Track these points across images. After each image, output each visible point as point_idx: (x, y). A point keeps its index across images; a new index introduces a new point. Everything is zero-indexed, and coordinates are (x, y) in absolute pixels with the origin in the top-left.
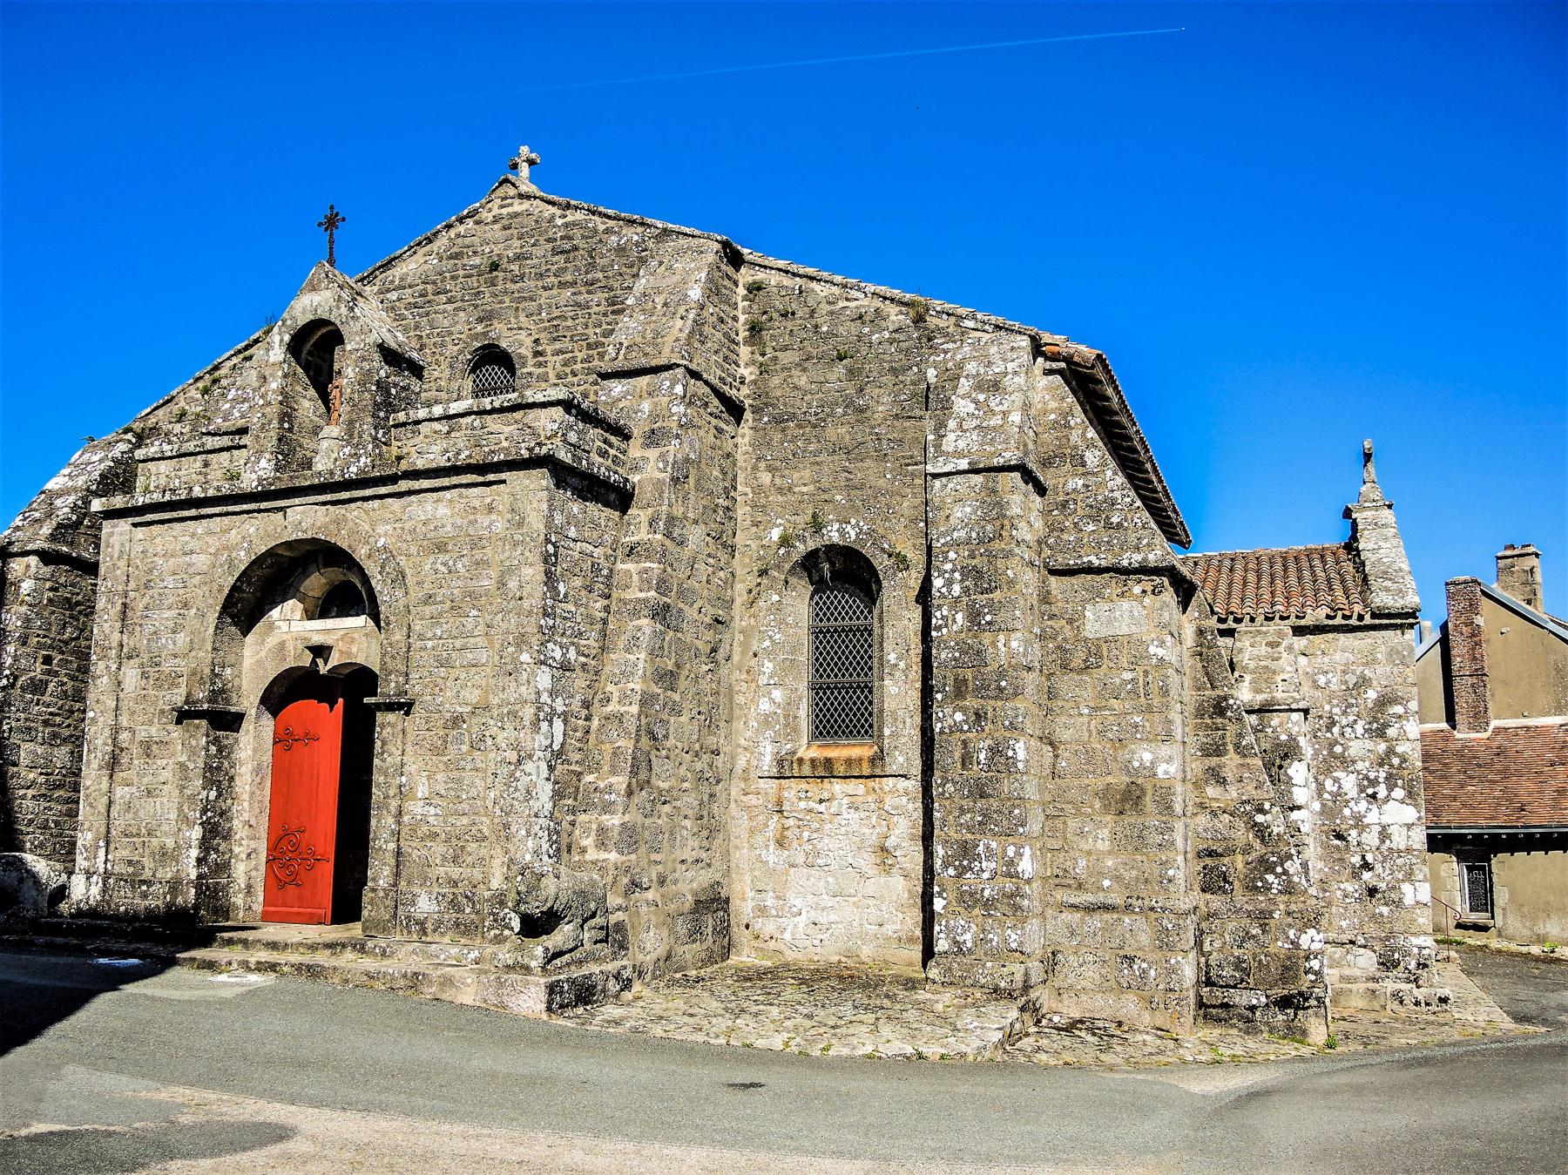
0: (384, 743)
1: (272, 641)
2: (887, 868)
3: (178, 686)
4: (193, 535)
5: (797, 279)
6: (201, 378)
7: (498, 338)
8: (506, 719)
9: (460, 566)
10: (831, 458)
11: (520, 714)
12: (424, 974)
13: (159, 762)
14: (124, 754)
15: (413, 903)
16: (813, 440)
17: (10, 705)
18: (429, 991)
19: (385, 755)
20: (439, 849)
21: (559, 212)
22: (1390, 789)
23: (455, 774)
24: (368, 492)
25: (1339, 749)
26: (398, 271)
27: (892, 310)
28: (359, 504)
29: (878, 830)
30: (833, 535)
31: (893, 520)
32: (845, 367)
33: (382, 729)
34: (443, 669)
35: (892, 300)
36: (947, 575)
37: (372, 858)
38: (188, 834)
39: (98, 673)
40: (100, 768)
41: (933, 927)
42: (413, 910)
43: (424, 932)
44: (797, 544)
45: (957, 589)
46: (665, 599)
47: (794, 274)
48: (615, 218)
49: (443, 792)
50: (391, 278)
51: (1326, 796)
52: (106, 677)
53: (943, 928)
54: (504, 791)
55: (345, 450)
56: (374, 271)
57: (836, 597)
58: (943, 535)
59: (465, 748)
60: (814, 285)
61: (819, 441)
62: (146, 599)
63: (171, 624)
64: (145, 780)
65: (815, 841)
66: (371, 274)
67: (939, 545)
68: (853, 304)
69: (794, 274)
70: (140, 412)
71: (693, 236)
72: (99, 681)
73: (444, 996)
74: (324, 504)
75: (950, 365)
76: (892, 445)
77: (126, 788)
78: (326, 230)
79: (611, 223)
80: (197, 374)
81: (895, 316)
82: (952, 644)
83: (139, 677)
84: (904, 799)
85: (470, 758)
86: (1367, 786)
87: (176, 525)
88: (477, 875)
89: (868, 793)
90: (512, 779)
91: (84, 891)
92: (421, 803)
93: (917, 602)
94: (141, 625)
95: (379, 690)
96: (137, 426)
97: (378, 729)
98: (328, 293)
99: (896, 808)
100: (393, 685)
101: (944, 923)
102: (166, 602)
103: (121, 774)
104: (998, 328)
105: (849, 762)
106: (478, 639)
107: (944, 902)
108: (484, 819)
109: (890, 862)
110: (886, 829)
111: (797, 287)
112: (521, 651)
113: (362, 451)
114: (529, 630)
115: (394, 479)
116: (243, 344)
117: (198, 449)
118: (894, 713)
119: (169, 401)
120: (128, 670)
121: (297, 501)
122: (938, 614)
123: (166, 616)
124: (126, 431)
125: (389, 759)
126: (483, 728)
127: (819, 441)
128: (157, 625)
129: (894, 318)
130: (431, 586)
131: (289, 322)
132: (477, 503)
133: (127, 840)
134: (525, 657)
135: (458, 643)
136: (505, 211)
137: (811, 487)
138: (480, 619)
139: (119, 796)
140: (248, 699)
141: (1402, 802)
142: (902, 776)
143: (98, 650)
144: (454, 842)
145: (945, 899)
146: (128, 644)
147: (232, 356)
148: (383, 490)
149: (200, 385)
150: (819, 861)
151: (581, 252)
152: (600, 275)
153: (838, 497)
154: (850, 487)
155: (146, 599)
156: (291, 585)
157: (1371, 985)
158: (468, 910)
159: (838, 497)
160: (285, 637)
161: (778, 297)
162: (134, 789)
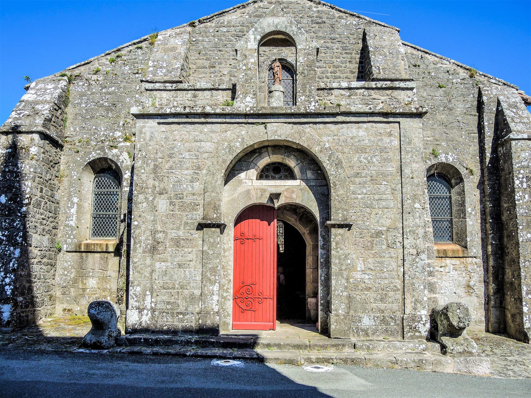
0: (337, 243)
1: (241, 189)
2: (470, 293)
3: (196, 210)
4: (201, 132)
5: (420, 52)
6: (109, 54)
7: (287, 56)
8: (408, 234)
9: (375, 160)
10: (439, 128)
11: (416, 232)
12: (426, 360)
13: (186, 250)
14: (160, 245)
15: (360, 321)
16: (430, 119)
17: (29, 214)
18: (429, 368)
19: (339, 250)
20: (371, 295)
23: (378, 259)
24: (318, 120)
26: (226, 18)
27: (461, 71)
28: (311, 125)
30: (442, 159)
31: (466, 155)
32: (443, 91)
34: (368, 209)
35: (461, 67)
36: (520, 179)
38: (211, 288)
39: (139, 200)
40: (144, 252)
42: (360, 324)
43: (367, 335)
44: (428, 161)
45: (525, 185)
47: (418, 50)
48: (344, 12)
49: (373, 268)
50: (222, 21)
52: (145, 204)
53: (528, 319)
54: (410, 268)
55: (301, 97)
56: (213, 16)
57: (433, 184)
58: (517, 163)
59: (384, 247)
60: (427, 55)
61: (433, 120)
62: (171, 163)
63: (189, 178)
64: (176, 259)
65: (439, 283)
66: (212, 17)
67: (516, 167)
69: (418, 50)
70: (68, 66)
71: (384, 26)
72: (140, 205)
73: (437, 370)
74: (289, 123)
75: (492, 96)
76: (464, 125)
77: (163, 263)
79: (341, 14)
80: (107, 52)
81: (463, 74)
82: (525, 207)
83: (168, 204)
84: (476, 266)
85: (387, 252)
87: (188, 126)
89: (461, 264)
90: (414, 262)
91: (138, 319)
92: (360, 273)
93: (477, 188)
94: (168, 177)
95: (332, 218)
96: (68, 73)
97: (333, 237)
98: (284, 19)
99: (472, 270)
100: (340, 215)
101: (527, 316)
102: (185, 166)
103: (159, 256)
104: (505, 84)
105: (453, 251)
106: (388, 196)
107: (527, 308)
108: (397, 281)
109: (471, 291)
110: (469, 278)
111: (420, 55)
112: (414, 203)
113: (312, 99)
114: (419, 193)
115: (337, 114)
116: (137, 41)
117: (190, 88)
118: (471, 232)
119: (88, 63)
120: (160, 201)
121: (272, 120)
122: (518, 194)
123: (185, 173)
124: (63, 76)
125: (341, 251)
126: (395, 238)
127: (433, 120)
128: (179, 177)
129: (462, 74)
130: (358, 169)
131: (259, 30)
133: (165, 291)
134: (417, 205)
135: (377, 197)
137: (432, 138)
138: (388, 186)
139: (158, 267)
140: (229, 219)
142: (475, 257)
143: (138, 188)
144: (380, 292)
145: (528, 307)
146: (159, 186)
147: (130, 45)
148: (327, 120)
149: (109, 57)
150: (442, 291)
151: (327, 24)
152: (338, 36)
153: (443, 144)
154: (447, 140)
155: (171, 163)
156: (252, 162)
158: (392, 324)
159: (443, 144)
160: (250, 188)
161: (412, 58)
162: (169, 264)
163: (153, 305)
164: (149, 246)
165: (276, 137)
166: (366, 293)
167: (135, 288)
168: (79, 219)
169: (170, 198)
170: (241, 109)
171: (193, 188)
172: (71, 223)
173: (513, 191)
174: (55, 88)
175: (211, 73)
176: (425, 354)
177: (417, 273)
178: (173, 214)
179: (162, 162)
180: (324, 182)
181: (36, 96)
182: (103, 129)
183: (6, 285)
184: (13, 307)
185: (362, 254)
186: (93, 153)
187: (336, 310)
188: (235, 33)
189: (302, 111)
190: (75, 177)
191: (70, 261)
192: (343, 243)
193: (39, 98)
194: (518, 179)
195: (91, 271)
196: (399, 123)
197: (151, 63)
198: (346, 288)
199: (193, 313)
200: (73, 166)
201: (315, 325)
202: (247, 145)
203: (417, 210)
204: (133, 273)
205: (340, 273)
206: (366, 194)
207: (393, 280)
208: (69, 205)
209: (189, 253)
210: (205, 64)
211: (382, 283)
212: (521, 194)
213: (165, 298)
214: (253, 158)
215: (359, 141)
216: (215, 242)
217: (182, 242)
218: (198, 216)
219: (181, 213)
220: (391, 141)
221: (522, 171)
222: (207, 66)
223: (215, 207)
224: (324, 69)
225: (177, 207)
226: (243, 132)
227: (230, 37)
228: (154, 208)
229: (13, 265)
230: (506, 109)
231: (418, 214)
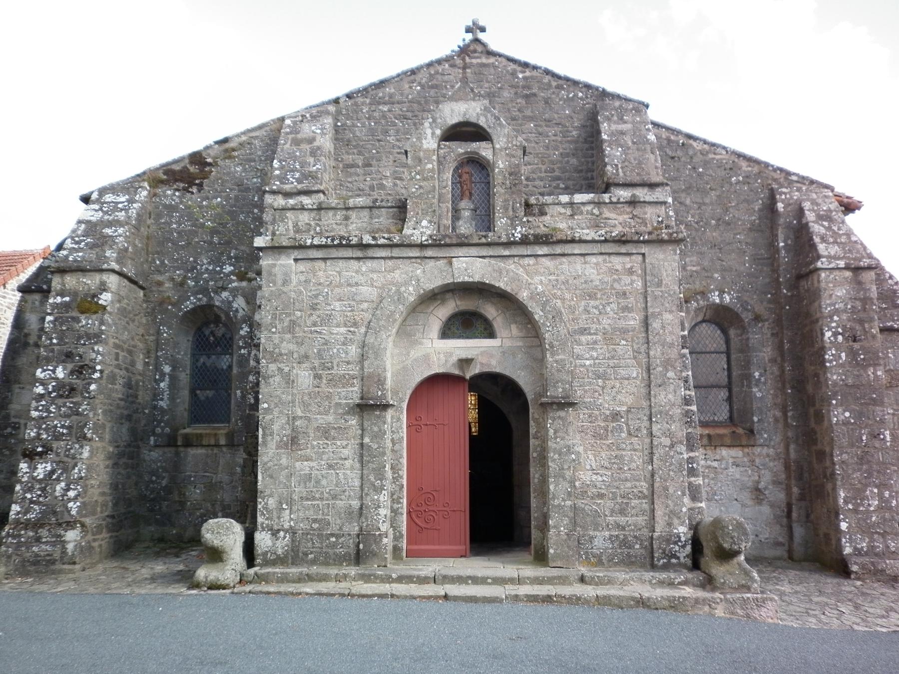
4: (357, 272)
9: (609, 309)
13: (339, 443)
19: (558, 440)
21: (519, 69)
28: (516, 259)
29: (752, 478)
33: (553, 421)
37: (553, 512)
40: (278, 447)
41: (256, 518)
59: (624, 435)
62: (314, 318)
68: (718, 157)
72: (271, 380)
84: (767, 459)
89: (744, 456)
100: (560, 390)
102: (335, 321)
112: (667, 371)
132: (619, 267)
134: (671, 374)
153: (716, 275)
156: (431, 313)
159: (716, 275)
160: (428, 351)
163: (292, 523)
164: (285, 439)
165: (466, 278)
166: (599, 502)
167: (265, 500)
168: (172, 398)
169: (315, 368)
170: (415, 238)
171: (347, 353)
172: (161, 403)
173: (823, 350)
174: (131, 201)
175: (365, 175)
176: (684, 589)
177: (671, 473)
178: (318, 392)
179: (301, 317)
180: (536, 341)
181: (101, 213)
182: (205, 261)
183: (70, 500)
184: (81, 533)
185: (593, 446)
186: (192, 298)
187: (555, 527)
188: (401, 113)
189: (504, 239)
190: (165, 335)
191: (160, 461)
192: (565, 430)
193: (106, 217)
194: (830, 329)
195: (193, 474)
196: (643, 255)
197: (276, 163)
198: (569, 494)
199: (349, 535)
200: (162, 318)
202: (424, 290)
203: (671, 381)
204: (263, 478)
205: (560, 475)
206: (597, 359)
207: (637, 484)
208: (157, 377)
209: (343, 448)
210: (356, 161)
211: (622, 487)
212: (834, 352)
213: (311, 514)
214: (418, 254)
215: (586, 282)
216: (380, 430)
217: (333, 432)
218: (353, 394)
219: (331, 391)
220: (632, 282)
221: (836, 318)
222: (360, 164)
223: (379, 380)
226: (419, 271)
227: (394, 120)
228: (289, 381)
229: (80, 471)
230: (813, 222)
231: (672, 387)
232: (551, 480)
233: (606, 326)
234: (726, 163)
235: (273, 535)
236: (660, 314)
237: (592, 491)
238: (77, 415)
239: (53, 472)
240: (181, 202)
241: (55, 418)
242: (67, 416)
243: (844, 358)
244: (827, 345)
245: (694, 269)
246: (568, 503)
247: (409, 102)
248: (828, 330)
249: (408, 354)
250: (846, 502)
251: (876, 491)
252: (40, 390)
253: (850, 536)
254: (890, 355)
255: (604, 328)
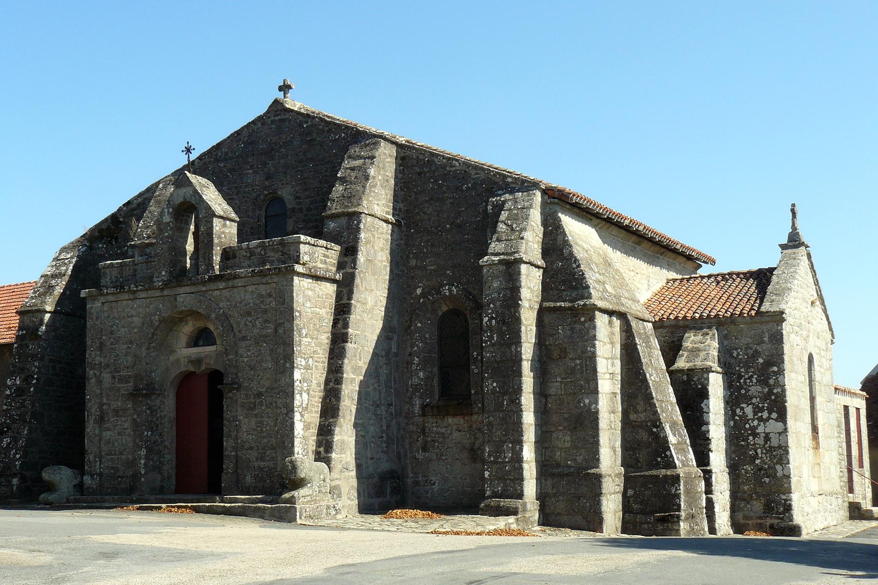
22: (770, 413)
25: (743, 392)
40: (94, 423)
46: (356, 332)
51: (737, 418)
62: (112, 340)
68: (452, 169)
78: (186, 154)
86: (757, 410)
88: (271, 464)
100: (230, 379)
136: (277, 118)
141: (776, 420)
153: (448, 272)
157: (759, 521)
159: (448, 272)
171: (127, 361)
201: (540, 523)
221: (492, 306)
224: (312, 199)
225: (117, 380)
228: (99, 381)
232: (225, 439)
233: (256, 335)
234: (460, 173)
235: (91, 477)
236: (283, 323)
237: (247, 445)
238: (24, 407)
239: (10, 443)
240: (106, 253)
241: (14, 410)
242: (19, 408)
243: (495, 339)
244: (485, 328)
245: (432, 268)
246: (233, 453)
247: (236, 157)
248: (485, 317)
249: (169, 359)
250: (489, 456)
251: (510, 445)
252: (8, 392)
253: (491, 483)
254: (560, 331)
255: (255, 336)
